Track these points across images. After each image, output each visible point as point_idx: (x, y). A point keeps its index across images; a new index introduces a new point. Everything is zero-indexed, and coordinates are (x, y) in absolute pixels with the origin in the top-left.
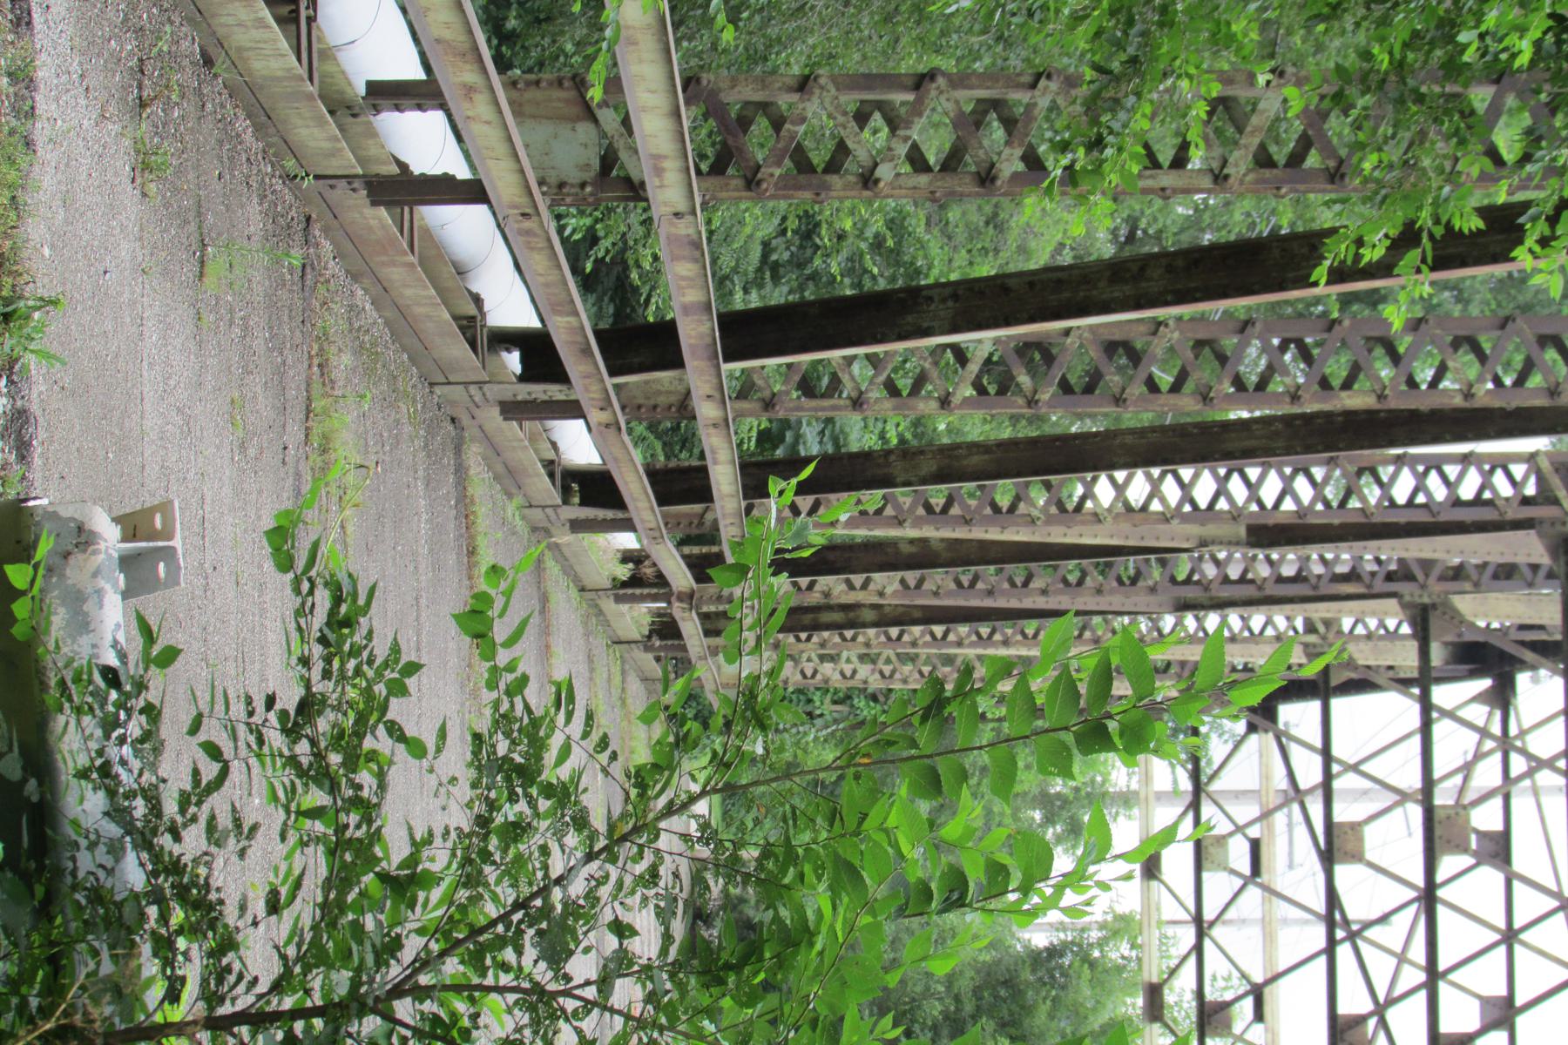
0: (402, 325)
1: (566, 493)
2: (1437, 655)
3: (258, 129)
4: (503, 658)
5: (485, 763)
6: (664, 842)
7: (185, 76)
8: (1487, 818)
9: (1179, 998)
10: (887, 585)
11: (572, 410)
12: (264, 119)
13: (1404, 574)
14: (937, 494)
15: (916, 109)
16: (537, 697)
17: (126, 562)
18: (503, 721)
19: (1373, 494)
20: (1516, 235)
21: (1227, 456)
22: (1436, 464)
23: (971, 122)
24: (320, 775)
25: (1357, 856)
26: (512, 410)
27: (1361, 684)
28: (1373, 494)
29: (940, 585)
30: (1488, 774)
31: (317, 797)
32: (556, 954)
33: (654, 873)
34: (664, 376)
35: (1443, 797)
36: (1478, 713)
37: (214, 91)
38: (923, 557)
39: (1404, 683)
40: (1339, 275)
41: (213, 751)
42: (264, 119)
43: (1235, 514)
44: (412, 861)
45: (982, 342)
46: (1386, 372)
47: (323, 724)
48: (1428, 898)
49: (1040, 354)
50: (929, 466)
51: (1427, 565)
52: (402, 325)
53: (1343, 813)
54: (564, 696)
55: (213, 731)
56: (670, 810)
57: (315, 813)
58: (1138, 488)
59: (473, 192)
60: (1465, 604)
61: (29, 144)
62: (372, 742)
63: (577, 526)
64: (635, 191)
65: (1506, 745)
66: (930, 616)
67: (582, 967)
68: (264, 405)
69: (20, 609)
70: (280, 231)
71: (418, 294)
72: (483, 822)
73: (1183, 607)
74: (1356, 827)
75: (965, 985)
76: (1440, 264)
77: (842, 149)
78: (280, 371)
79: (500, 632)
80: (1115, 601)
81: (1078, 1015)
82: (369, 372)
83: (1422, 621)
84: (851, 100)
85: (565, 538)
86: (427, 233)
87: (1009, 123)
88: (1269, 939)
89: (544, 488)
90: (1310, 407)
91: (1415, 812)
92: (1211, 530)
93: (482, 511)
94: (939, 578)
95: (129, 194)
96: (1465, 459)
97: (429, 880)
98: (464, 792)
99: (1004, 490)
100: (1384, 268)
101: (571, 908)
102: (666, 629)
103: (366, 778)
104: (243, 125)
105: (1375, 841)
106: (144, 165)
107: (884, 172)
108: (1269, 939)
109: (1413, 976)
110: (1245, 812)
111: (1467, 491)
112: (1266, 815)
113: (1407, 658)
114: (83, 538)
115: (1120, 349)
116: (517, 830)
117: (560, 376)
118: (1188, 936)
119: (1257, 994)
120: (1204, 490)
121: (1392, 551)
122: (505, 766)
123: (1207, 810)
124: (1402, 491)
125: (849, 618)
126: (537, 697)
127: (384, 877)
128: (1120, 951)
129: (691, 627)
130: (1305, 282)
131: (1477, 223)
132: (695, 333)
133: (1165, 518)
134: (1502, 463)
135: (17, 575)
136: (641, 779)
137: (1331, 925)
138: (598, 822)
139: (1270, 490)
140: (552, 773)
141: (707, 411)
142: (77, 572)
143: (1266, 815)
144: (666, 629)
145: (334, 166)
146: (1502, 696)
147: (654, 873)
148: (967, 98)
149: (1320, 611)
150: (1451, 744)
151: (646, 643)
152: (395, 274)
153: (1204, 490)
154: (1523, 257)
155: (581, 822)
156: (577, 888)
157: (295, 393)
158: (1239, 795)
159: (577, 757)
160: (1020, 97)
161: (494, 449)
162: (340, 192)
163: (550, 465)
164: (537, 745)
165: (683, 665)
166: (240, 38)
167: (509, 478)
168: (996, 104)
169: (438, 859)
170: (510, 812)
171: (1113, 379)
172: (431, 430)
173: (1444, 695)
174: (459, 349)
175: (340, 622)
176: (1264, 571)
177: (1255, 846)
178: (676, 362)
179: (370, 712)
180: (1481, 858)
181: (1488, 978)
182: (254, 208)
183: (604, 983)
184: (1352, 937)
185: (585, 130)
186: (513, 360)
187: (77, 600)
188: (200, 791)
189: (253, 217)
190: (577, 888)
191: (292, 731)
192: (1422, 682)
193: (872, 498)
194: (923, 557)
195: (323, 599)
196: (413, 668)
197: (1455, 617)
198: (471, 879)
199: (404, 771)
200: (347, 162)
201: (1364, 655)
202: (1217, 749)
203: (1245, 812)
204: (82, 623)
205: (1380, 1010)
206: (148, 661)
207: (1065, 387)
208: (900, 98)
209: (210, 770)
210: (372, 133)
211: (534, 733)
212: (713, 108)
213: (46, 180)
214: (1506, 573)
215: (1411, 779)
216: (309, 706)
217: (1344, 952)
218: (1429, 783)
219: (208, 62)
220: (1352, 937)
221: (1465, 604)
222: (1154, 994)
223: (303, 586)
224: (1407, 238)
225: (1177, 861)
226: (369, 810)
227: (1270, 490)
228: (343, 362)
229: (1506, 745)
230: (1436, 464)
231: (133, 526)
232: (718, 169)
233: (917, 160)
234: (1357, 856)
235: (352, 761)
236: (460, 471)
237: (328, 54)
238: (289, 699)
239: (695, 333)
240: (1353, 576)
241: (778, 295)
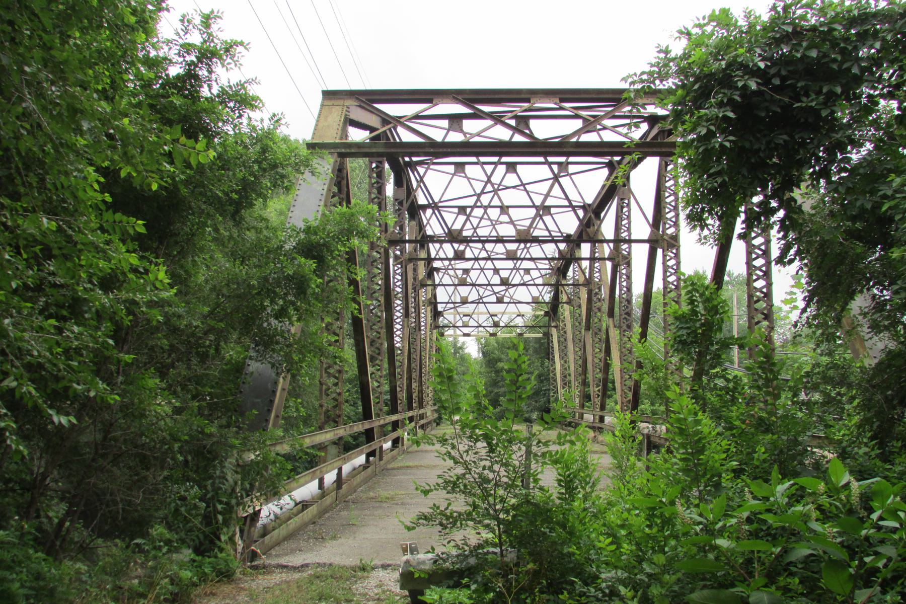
0: (365, 481)
1: (397, 447)
2: (429, 282)
3: (327, 512)
4: (433, 487)
5: (453, 491)
6: (468, 459)
7: (317, 528)
8: (460, 273)
9: (491, 330)
10: (415, 385)
11: (381, 447)
12: (325, 511)
13: (414, 289)
14: (398, 377)
15: (326, 384)
16: (441, 481)
17: (412, 553)
18: (445, 488)
19: (400, 295)
20: (355, 279)
21: (392, 323)
22: (394, 283)
23: (329, 375)
24: (454, 523)
25: (467, 298)
26: (381, 459)
27: (435, 296)
28: (400, 295)
29: (415, 375)
30: (451, 272)
31: (458, 524)
32: (489, 481)
33: (474, 462)
34: (375, 430)
35: (456, 283)
36: (441, 274)
37: (321, 521)
38: (410, 379)
39: (435, 289)
40: (361, 314)
41: (449, 542)
42: (325, 511)
43: (403, 321)
44: (470, 505)
45: (370, 370)
46: (377, 294)
47: (444, 522)
48: (473, 285)
49: (372, 359)
50: (393, 378)
51: (413, 284)
52: (365, 481)
53: (458, 300)
54: (440, 476)
55: (445, 542)
56: (462, 458)
57: (461, 524)
58: (397, 339)
59: (340, 470)
60: (421, 277)
61: (331, 565)
62: (448, 512)
63: (403, 445)
64: (341, 438)
65: (447, 269)
66: (421, 377)
67: (491, 476)
68: (380, 511)
69: (423, 576)
70: (347, 508)
71: (359, 478)
72: (463, 493)
73: (420, 329)
74: (461, 298)
75: (489, 370)
76: (359, 294)
77: (334, 399)
78: (373, 507)
79: (428, 488)
80: (418, 342)
81: (495, 348)
82: (373, 488)
83: (424, 285)
84: (324, 396)
85: (405, 447)
86: (347, 477)
87: (329, 367)
88: (481, 313)
89: (395, 452)
90: (383, 308)
91: (458, 288)
92: (406, 325)
93: (400, 464)
94: (414, 375)
95: (340, 540)
96: (394, 278)
97: (474, 502)
98: (458, 496)
99: (397, 364)
100: (359, 304)
101: (480, 477)
102: (422, 427)
103: (455, 514)
104: (327, 515)
105: (464, 294)
106: (334, 538)
107: (338, 391)
108: (481, 313)
109: (489, 288)
110: (458, 317)
111: (399, 278)
112: (458, 313)
113: (430, 288)
114: (407, 562)
115: (372, 343)
116: (465, 486)
117: (375, 451)
118: (481, 329)
119: (492, 316)
120: (398, 327)
121: (410, 290)
122: (453, 488)
123: (457, 324)
124: (399, 290)
125: (421, 392)
126: (441, 481)
127: (474, 510)
128: (483, 341)
129: (422, 422)
130: (361, 320)
131: (352, 287)
132: (367, 425)
133: (403, 334)
134: (394, 271)
135: (416, 575)
136: (456, 462)
137: (479, 303)
138: (464, 471)
139: (399, 314)
140: (455, 478)
141: (382, 422)
142: (414, 563)
143: (458, 313)
144: (422, 427)
145: (335, 497)
146: (438, 270)
147: (474, 462)
148: (324, 375)
149: (421, 304)
150: (447, 280)
151: (425, 430)
152: (355, 483)
153: (398, 327)
154: (358, 279)
155: (464, 475)
156: (476, 476)
157: (377, 505)
158: (455, 317)
159: (452, 474)
160: (325, 366)
161: (388, 462)
162: (339, 495)
163: (392, 450)
164: (450, 481)
165: (429, 423)
166: (310, 516)
167: (394, 458)
168: (326, 369)
169: (470, 500)
170: (462, 487)
171: (378, 345)
172: (384, 475)
173: (437, 281)
174: (369, 470)
175: (426, 518)
176: (413, 315)
177: (464, 316)
178: (373, 429)
179: (442, 513)
180: (468, 275)
181: (489, 273)
182: (342, 513)
183: (494, 472)
184: (482, 298)
185: (329, 448)
186: (371, 458)
187: (419, 563)
188: (457, 546)
189: (344, 513)
190: (476, 476)
191: (446, 528)
192: (435, 286)
193: (398, 389)
194: (409, 386)
195: (421, 521)
196: (434, 505)
197: (423, 279)
198: (474, 495)
199: (453, 507)
200: (334, 494)
201: (429, 296)
202: (446, 322)
203: (458, 317)
204: (423, 562)
205: (495, 293)
206: (433, 552)
207: (379, 354)
208: (324, 387)
209: (452, 543)
210: (328, 489)
211: (447, 482)
212: (326, 422)
213: (337, 560)
214: (415, 270)
215: (453, 288)
216: (441, 524)
217: (485, 300)
218: (454, 285)
219: (314, 523)
220: (482, 298)
221: (421, 277)
222: (491, 335)
223: (418, 524)
224: (354, 300)
225: (466, 330)
226: (460, 514)
227: (399, 314)
228: (372, 494)
229: (447, 269)
230: (394, 283)
231: (405, 551)
232: (336, 422)
233: (336, 384)
234: (467, 298)
235: (451, 516)
236: (393, 469)
237: (313, 498)
238: (440, 528)
239: (367, 425)
240: (415, 298)
241: (360, 403)
